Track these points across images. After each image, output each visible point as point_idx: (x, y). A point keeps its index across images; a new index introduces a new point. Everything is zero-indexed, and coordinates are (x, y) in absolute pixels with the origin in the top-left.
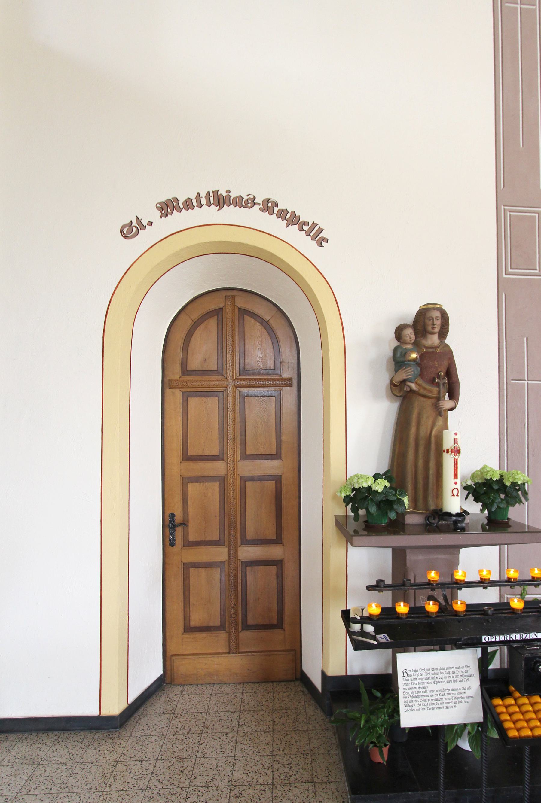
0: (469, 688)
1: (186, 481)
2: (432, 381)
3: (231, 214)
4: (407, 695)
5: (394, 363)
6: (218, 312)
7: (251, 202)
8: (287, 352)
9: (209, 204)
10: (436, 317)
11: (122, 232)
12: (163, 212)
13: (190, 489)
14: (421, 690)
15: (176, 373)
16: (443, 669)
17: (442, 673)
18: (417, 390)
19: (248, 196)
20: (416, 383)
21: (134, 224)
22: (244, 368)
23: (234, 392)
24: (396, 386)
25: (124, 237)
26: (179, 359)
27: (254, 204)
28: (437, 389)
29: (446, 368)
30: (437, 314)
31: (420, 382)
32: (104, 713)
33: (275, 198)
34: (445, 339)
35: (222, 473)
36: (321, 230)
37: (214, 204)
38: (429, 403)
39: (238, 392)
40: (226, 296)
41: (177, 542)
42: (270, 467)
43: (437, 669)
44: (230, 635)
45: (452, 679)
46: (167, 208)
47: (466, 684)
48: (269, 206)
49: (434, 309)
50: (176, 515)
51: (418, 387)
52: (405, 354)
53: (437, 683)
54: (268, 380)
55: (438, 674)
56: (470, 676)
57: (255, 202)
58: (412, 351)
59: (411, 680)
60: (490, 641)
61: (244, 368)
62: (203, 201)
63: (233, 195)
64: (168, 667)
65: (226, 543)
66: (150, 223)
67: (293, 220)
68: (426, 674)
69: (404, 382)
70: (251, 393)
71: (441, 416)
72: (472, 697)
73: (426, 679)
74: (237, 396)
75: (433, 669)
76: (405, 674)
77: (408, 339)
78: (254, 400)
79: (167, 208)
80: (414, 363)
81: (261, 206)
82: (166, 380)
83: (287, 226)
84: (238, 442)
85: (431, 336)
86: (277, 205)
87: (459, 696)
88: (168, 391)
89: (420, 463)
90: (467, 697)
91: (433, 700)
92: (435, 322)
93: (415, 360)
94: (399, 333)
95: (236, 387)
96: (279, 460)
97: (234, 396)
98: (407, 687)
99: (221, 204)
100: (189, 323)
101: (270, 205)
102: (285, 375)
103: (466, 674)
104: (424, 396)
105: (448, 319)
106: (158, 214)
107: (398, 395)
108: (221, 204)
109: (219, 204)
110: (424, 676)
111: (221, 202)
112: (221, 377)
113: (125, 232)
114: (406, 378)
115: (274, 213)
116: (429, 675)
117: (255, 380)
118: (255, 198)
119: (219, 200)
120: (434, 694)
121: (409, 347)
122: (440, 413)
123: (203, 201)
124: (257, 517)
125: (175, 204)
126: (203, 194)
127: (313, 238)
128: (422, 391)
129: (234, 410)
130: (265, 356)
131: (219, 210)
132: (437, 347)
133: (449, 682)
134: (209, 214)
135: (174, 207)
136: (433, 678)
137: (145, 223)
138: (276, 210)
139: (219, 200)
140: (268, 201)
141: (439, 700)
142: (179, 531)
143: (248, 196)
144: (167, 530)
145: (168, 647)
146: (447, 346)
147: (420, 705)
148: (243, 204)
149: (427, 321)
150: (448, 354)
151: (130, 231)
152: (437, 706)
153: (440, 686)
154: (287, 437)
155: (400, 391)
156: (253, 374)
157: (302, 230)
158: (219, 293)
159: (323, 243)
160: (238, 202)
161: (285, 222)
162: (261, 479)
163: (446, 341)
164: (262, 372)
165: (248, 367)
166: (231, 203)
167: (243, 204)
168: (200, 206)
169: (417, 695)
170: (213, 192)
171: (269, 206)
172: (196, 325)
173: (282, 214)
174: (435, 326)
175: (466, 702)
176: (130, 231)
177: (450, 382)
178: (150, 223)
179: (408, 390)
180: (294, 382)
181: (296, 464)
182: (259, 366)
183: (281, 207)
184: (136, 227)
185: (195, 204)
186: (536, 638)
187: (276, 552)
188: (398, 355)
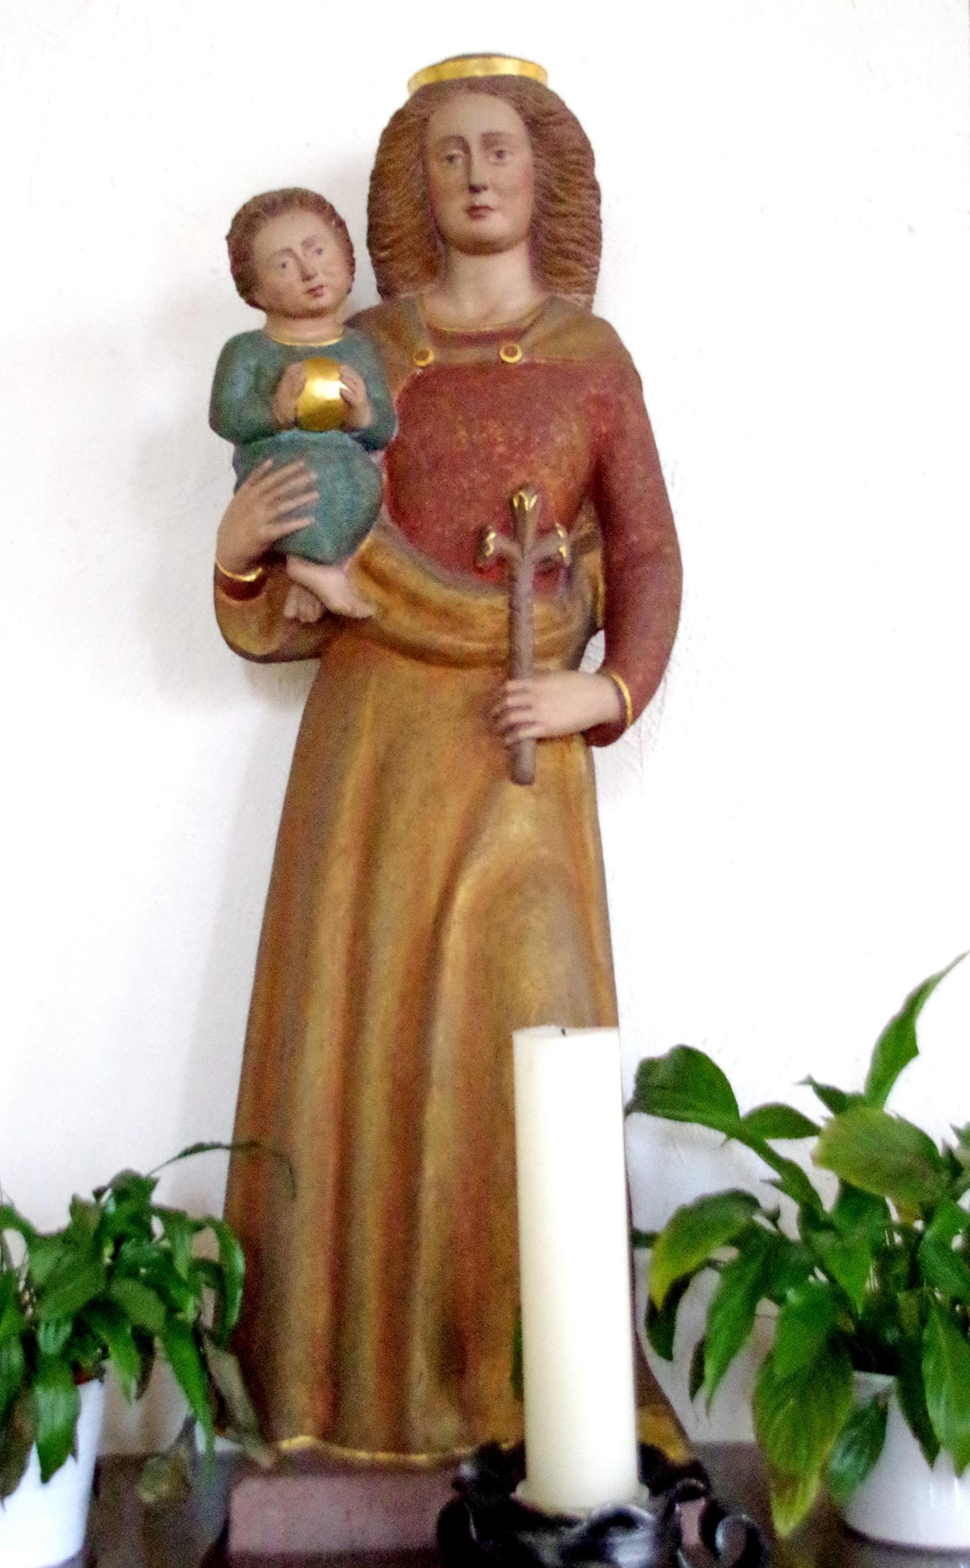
2: (469, 559)
10: (490, 141)
18: (363, 610)
20: (365, 567)
28: (500, 601)
29: (584, 464)
30: (502, 118)
31: (394, 555)
49: (474, 85)
51: (375, 592)
58: (323, 358)
69: (272, 557)
71: (520, 780)
93: (338, 417)
104: (421, 654)
107: (258, 651)
114: (275, 531)
128: (403, 623)
132: (514, 334)
149: (436, 167)
150: (610, 385)
177: (617, 557)
179: (311, 613)
188: (240, 388)
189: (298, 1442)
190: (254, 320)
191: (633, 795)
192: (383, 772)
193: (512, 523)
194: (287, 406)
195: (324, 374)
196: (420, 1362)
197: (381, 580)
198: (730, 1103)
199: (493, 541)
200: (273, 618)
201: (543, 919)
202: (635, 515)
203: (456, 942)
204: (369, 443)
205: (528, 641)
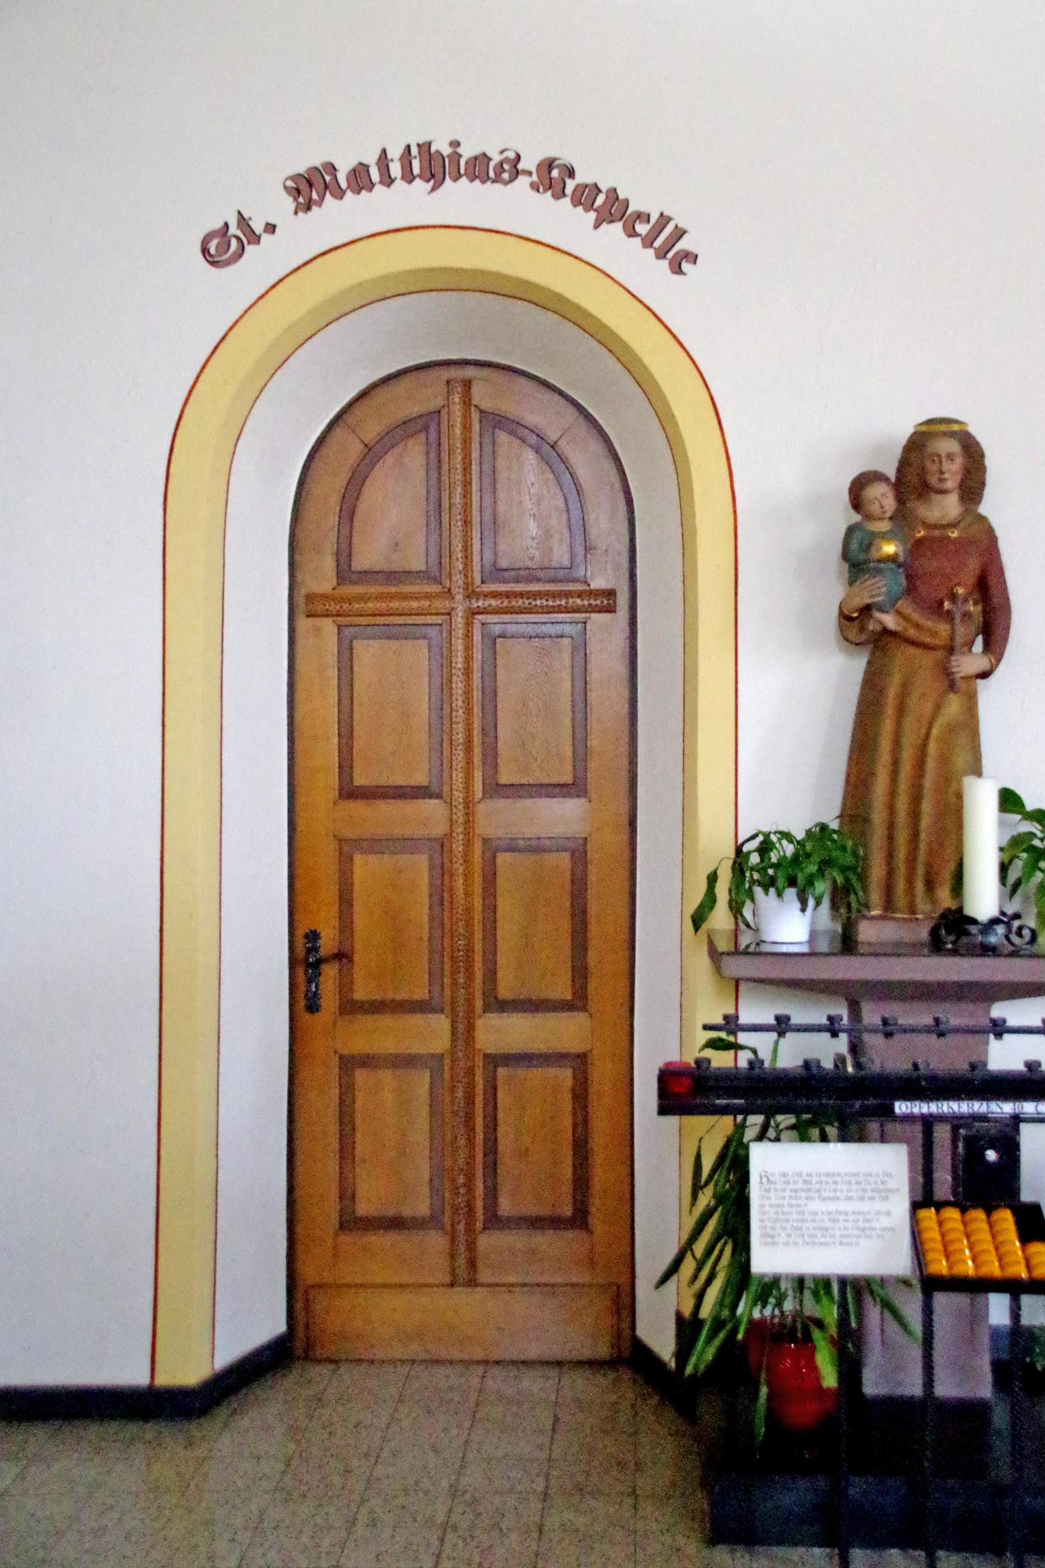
0: (888, 1214)
1: (346, 851)
2: (936, 609)
3: (461, 200)
4: (764, 1217)
5: (846, 566)
6: (426, 424)
7: (510, 169)
8: (604, 523)
9: (409, 177)
10: (950, 457)
11: (205, 251)
12: (301, 200)
13: (357, 870)
14: (794, 1210)
15: (322, 578)
16: (839, 1175)
17: (836, 1183)
18: (899, 629)
19: (502, 152)
20: (898, 613)
21: (233, 230)
22: (494, 564)
23: (469, 624)
24: (850, 619)
25: (213, 263)
26: (330, 544)
27: (516, 173)
28: (947, 627)
29: (977, 572)
30: (953, 446)
31: (906, 606)
32: (163, 1380)
33: (566, 156)
34: (979, 502)
35: (439, 829)
36: (680, 233)
37: (420, 176)
38: (927, 660)
39: (477, 626)
40: (448, 382)
41: (323, 1003)
42: (563, 817)
43: (828, 1175)
44: (453, 1240)
45: (854, 1194)
46: (310, 188)
47: (879, 1205)
48: (553, 177)
50: (322, 934)
51: (903, 622)
52: (869, 546)
53: (824, 1199)
54: (554, 595)
55: (827, 1183)
56: (890, 1191)
57: (520, 166)
58: (885, 536)
59: (776, 1190)
60: (909, 1111)
61: (494, 564)
62: (396, 169)
63: (467, 152)
64: (301, 1318)
65: (448, 1009)
66: (271, 228)
67: (612, 209)
68: (805, 1182)
69: (867, 610)
70: (511, 629)
72: (892, 1229)
73: (803, 1190)
74: (477, 637)
75: (818, 1175)
76: (765, 1180)
77: (875, 508)
78: (518, 647)
79: (310, 188)
80: (893, 566)
81: (535, 178)
82: (302, 592)
83: (597, 226)
84: (477, 751)
85: (939, 497)
86: (571, 173)
87: (867, 1225)
88: (303, 623)
89: (902, 804)
90: (884, 1229)
91: (814, 1229)
92: (946, 466)
93: (893, 559)
94: (858, 490)
95: (474, 614)
96: (583, 800)
97: (468, 636)
98: (767, 1203)
99: (439, 176)
100: (355, 450)
101: (555, 173)
102: (598, 583)
103: (881, 1187)
105: (982, 456)
106: (289, 203)
108: (439, 176)
109: (433, 176)
110: (800, 1186)
111: (437, 170)
112: (435, 588)
113: (213, 251)
114: (869, 601)
115: (564, 195)
116: (809, 1185)
117: (521, 595)
118: (518, 157)
119: (433, 166)
120: (817, 1218)
121: (884, 526)
122: (962, 689)
123: (396, 169)
124: (527, 947)
125: (328, 178)
126: (395, 153)
127: (661, 254)
128: (912, 633)
129: (468, 671)
130: (548, 534)
131: (433, 189)
133: (849, 1199)
134: (407, 201)
135: (326, 187)
136: (818, 1191)
137: (258, 227)
138: (571, 185)
139: (433, 166)
140: (548, 165)
141: (827, 1229)
142: (330, 972)
143: (502, 152)
144: (300, 971)
145: (299, 1265)
146: (983, 520)
147: (789, 1235)
148: (492, 174)
149: (928, 463)
151: (223, 247)
152: (823, 1240)
153: (831, 1206)
154: (604, 738)
155: (862, 629)
156: (517, 581)
157: (632, 233)
158: (434, 373)
159: (685, 266)
160: (479, 169)
161: (593, 215)
162: (537, 848)
163: (983, 509)
164: (540, 574)
165: (504, 563)
166: (462, 171)
167: (492, 174)
168: (388, 181)
169: (784, 1217)
170: (419, 146)
171: (553, 177)
172: (372, 455)
173: (584, 197)
174: (946, 476)
175: (878, 1236)
176: (223, 247)
178: (271, 228)
179: (879, 628)
180: (619, 601)
181: (624, 808)
182: (532, 559)
183: (583, 176)
184: (238, 238)
185: (375, 175)
186: (999, 1110)
187: (566, 1032)
188: (854, 546)
189: (875, 912)
190: (856, 518)
191: (991, 698)
192: (905, 685)
193: (953, 597)
194: (874, 554)
195: (889, 544)
196: (920, 886)
197: (906, 618)
198: (1023, 806)
199: (947, 605)
200: (862, 629)
201: (963, 740)
202: (994, 591)
203: (932, 748)
204: (900, 566)
205: (959, 640)
